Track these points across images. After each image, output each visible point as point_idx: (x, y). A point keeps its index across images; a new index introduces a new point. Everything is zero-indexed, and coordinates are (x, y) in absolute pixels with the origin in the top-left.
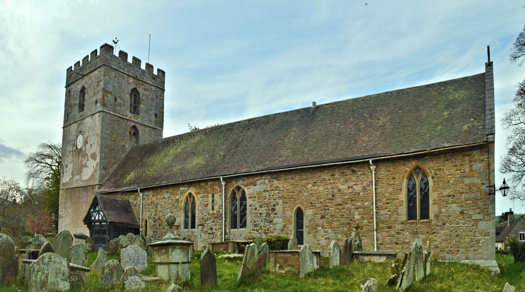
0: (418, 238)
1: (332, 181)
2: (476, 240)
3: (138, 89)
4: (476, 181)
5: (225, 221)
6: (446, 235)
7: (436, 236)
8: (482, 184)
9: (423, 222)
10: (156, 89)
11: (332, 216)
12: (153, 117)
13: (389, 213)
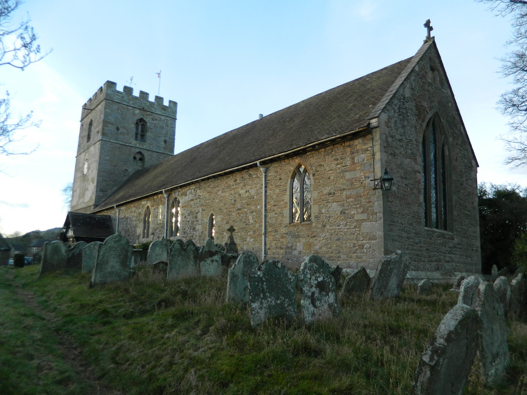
1: (235, 186)
2: (360, 245)
3: (145, 119)
4: (358, 175)
5: (167, 230)
6: (326, 239)
8: (365, 177)
9: (304, 224)
11: (234, 221)
12: (163, 143)
13: (276, 215)
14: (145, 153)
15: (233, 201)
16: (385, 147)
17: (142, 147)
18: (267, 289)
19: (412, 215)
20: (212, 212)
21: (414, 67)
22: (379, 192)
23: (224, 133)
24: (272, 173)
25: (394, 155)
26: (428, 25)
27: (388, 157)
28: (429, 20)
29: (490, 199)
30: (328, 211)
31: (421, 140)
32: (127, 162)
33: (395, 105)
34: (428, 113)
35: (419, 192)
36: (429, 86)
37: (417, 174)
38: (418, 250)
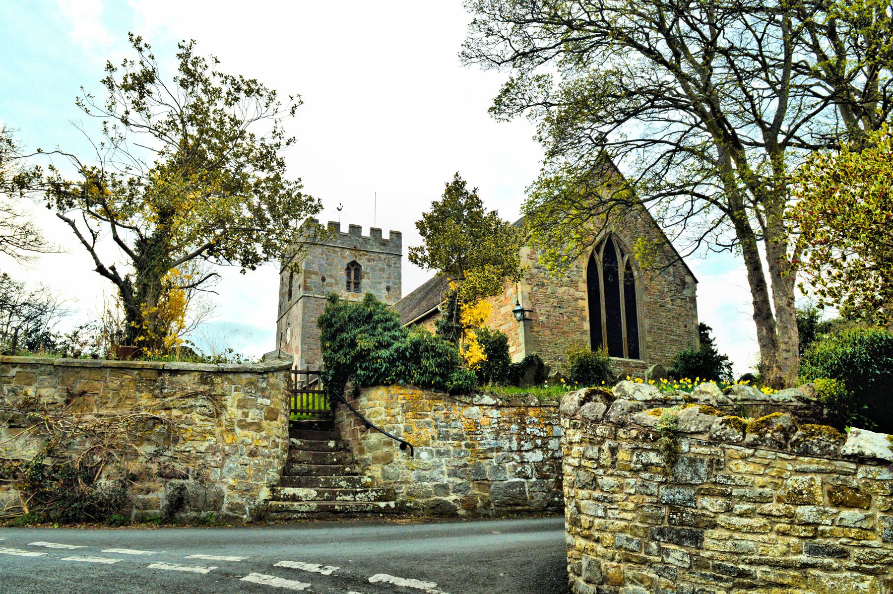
3: (358, 261)
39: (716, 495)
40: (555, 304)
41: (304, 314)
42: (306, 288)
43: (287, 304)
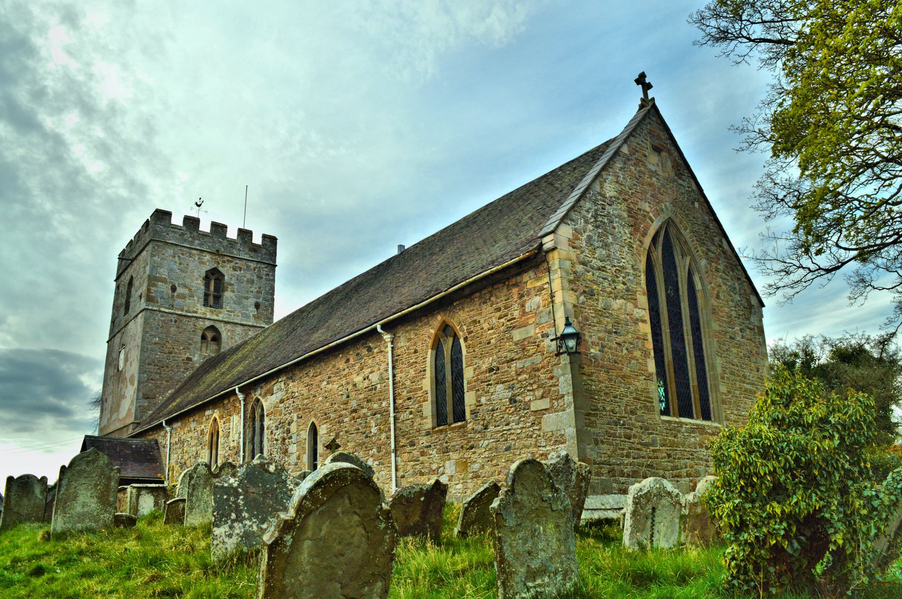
0: (449, 459)
3: (220, 269)
4: (532, 334)
7: (474, 453)
10: (259, 265)
11: (346, 432)
13: (411, 416)
14: (222, 328)
15: (344, 397)
16: (570, 282)
17: (215, 317)
18: (244, 505)
19: (634, 395)
20: (313, 420)
21: (619, 147)
22: (565, 359)
23: (344, 282)
24: (402, 343)
25: (590, 294)
26: (641, 80)
27: (578, 298)
28: (643, 73)
29: (821, 367)
30: (489, 400)
31: (642, 266)
32: (190, 344)
33: (588, 211)
34: (652, 221)
35: (646, 355)
36: (651, 177)
37: (640, 324)
38: (650, 458)
39: (513, 484)
40: (610, 327)
41: (145, 332)
42: (150, 299)
43: (122, 318)
